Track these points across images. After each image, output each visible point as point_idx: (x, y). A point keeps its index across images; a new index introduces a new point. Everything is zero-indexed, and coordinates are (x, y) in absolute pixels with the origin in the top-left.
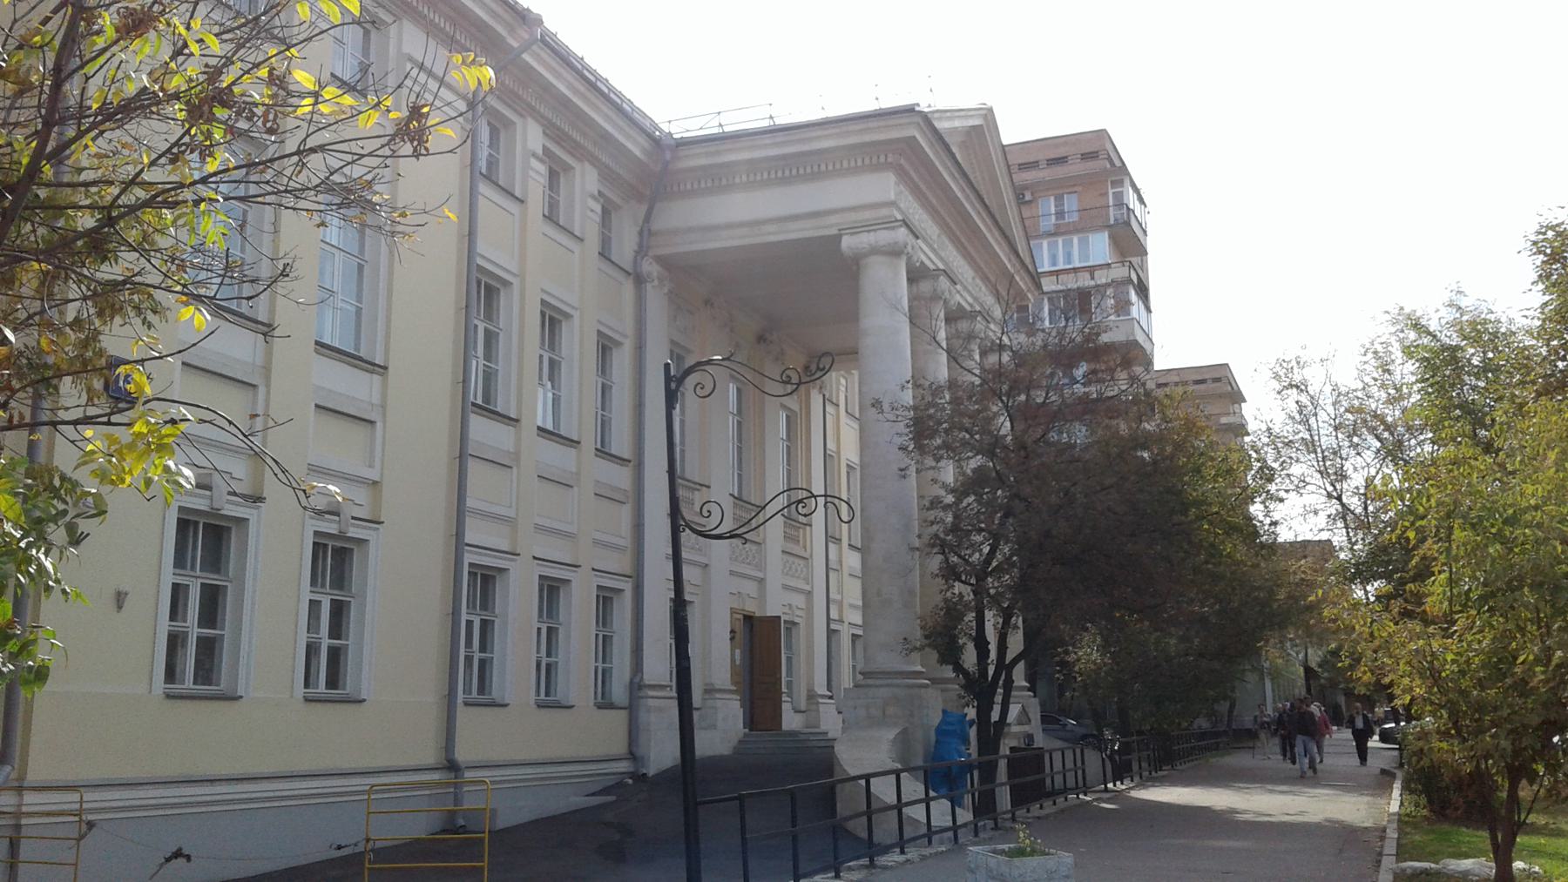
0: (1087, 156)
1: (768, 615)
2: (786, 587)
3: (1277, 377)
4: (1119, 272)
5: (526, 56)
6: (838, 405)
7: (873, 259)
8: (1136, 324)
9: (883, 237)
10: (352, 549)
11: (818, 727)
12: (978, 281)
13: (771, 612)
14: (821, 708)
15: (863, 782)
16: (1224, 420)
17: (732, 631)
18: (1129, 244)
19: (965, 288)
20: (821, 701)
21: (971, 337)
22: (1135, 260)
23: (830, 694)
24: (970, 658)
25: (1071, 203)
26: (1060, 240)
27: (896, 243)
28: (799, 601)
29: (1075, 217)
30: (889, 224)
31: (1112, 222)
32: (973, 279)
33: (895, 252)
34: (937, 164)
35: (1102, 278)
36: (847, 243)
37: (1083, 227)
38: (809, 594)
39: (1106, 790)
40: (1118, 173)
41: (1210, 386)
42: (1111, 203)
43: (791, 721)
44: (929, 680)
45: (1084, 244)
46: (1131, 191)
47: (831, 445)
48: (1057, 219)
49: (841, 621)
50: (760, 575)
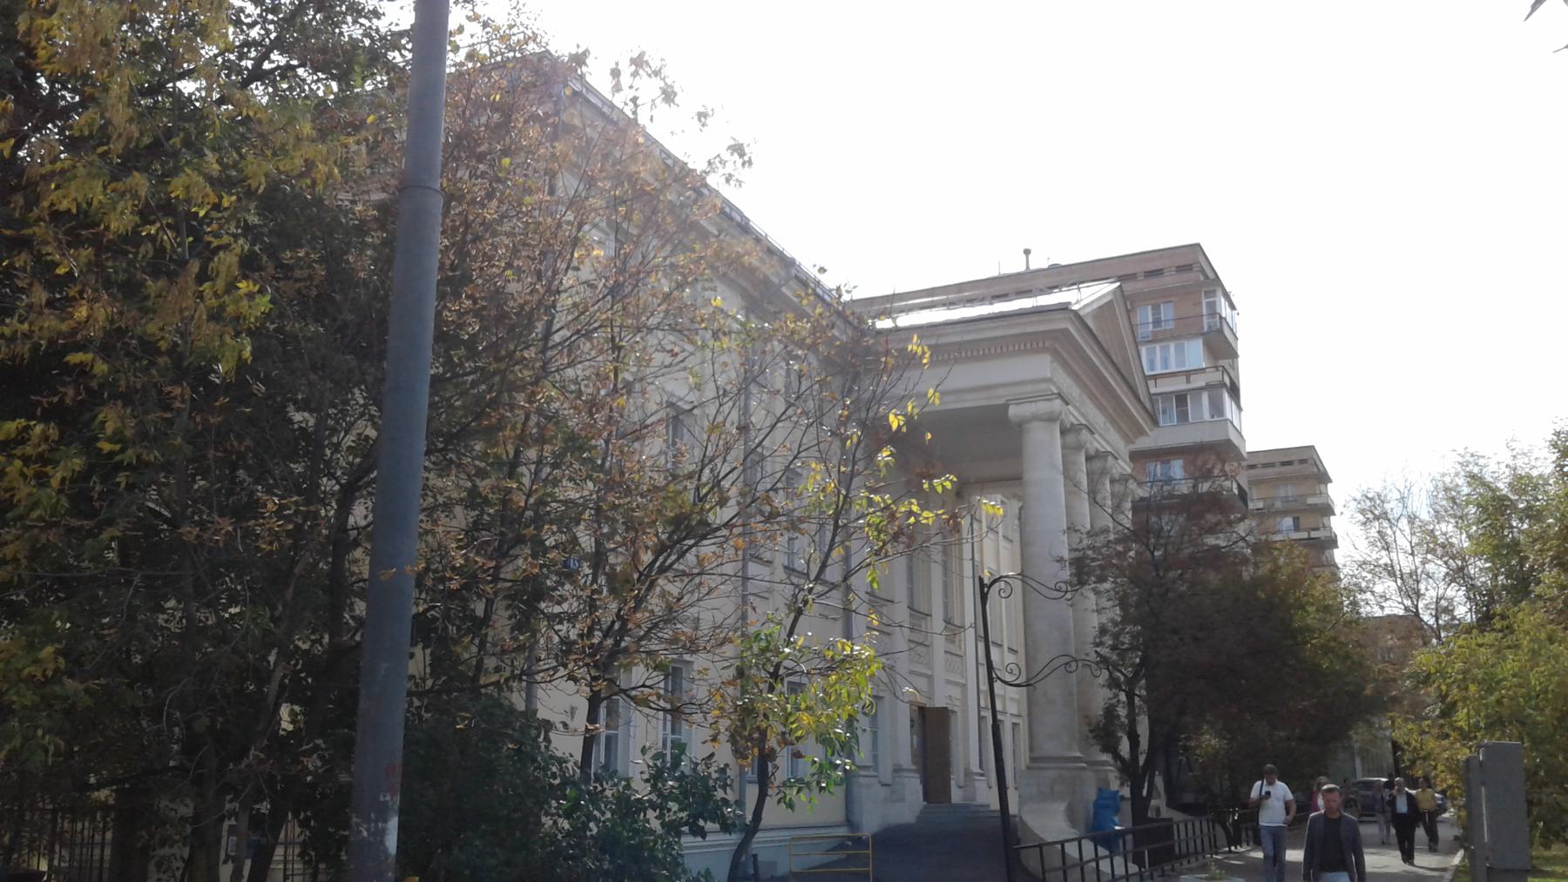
0: (1182, 269)
1: (937, 706)
2: (949, 682)
3: (1362, 512)
4: (1214, 377)
5: (784, 289)
6: (997, 533)
7: (1035, 425)
8: (1229, 424)
9: (1042, 407)
10: (681, 669)
11: (974, 799)
12: (1108, 425)
13: (939, 702)
14: (977, 784)
15: (1059, 846)
16: (1311, 501)
17: (912, 721)
18: (1221, 348)
19: (1101, 436)
20: (977, 778)
21: (1104, 472)
22: (1224, 362)
23: (980, 771)
24: (1125, 748)
25: (1167, 312)
26: (1158, 347)
27: (1052, 412)
28: (956, 692)
29: (1171, 325)
30: (1047, 397)
31: (1206, 329)
32: (1080, 395)
33: (1051, 418)
34: (1110, 380)
35: (1198, 381)
36: (1013, 411)
37: (1178, 335)
38: (964, 686)
39: (1230, 851)
40: (1212, 283)
41: (1297, 467)
42: (1205, 312)
43: (956, 796)
44: (1086, 763)
45: (1180, 351)
46: (1223, 300)
47: (977, 557)
48: (1154, 327)
49: (1004, 713)
50: (929, 673)
